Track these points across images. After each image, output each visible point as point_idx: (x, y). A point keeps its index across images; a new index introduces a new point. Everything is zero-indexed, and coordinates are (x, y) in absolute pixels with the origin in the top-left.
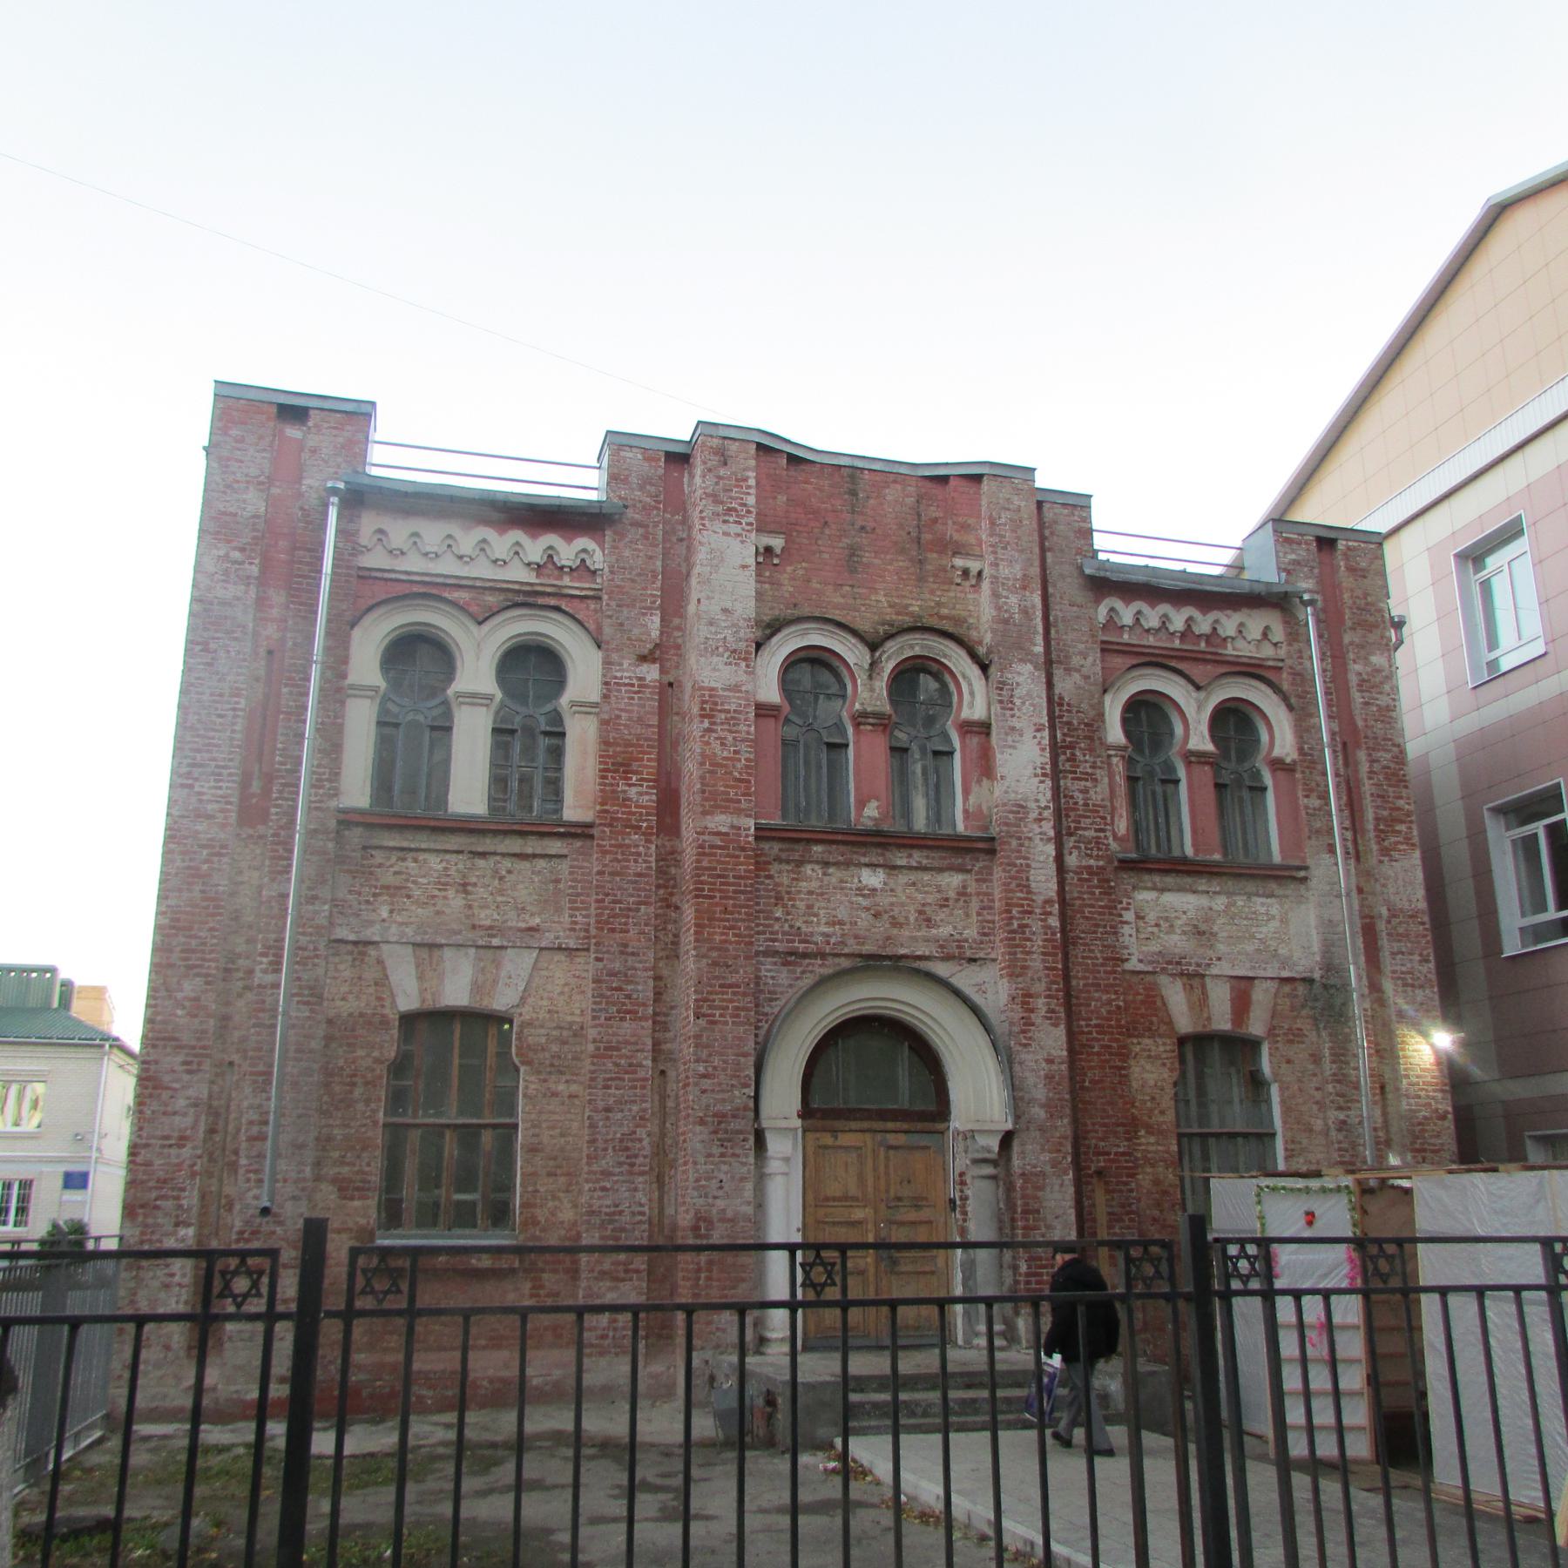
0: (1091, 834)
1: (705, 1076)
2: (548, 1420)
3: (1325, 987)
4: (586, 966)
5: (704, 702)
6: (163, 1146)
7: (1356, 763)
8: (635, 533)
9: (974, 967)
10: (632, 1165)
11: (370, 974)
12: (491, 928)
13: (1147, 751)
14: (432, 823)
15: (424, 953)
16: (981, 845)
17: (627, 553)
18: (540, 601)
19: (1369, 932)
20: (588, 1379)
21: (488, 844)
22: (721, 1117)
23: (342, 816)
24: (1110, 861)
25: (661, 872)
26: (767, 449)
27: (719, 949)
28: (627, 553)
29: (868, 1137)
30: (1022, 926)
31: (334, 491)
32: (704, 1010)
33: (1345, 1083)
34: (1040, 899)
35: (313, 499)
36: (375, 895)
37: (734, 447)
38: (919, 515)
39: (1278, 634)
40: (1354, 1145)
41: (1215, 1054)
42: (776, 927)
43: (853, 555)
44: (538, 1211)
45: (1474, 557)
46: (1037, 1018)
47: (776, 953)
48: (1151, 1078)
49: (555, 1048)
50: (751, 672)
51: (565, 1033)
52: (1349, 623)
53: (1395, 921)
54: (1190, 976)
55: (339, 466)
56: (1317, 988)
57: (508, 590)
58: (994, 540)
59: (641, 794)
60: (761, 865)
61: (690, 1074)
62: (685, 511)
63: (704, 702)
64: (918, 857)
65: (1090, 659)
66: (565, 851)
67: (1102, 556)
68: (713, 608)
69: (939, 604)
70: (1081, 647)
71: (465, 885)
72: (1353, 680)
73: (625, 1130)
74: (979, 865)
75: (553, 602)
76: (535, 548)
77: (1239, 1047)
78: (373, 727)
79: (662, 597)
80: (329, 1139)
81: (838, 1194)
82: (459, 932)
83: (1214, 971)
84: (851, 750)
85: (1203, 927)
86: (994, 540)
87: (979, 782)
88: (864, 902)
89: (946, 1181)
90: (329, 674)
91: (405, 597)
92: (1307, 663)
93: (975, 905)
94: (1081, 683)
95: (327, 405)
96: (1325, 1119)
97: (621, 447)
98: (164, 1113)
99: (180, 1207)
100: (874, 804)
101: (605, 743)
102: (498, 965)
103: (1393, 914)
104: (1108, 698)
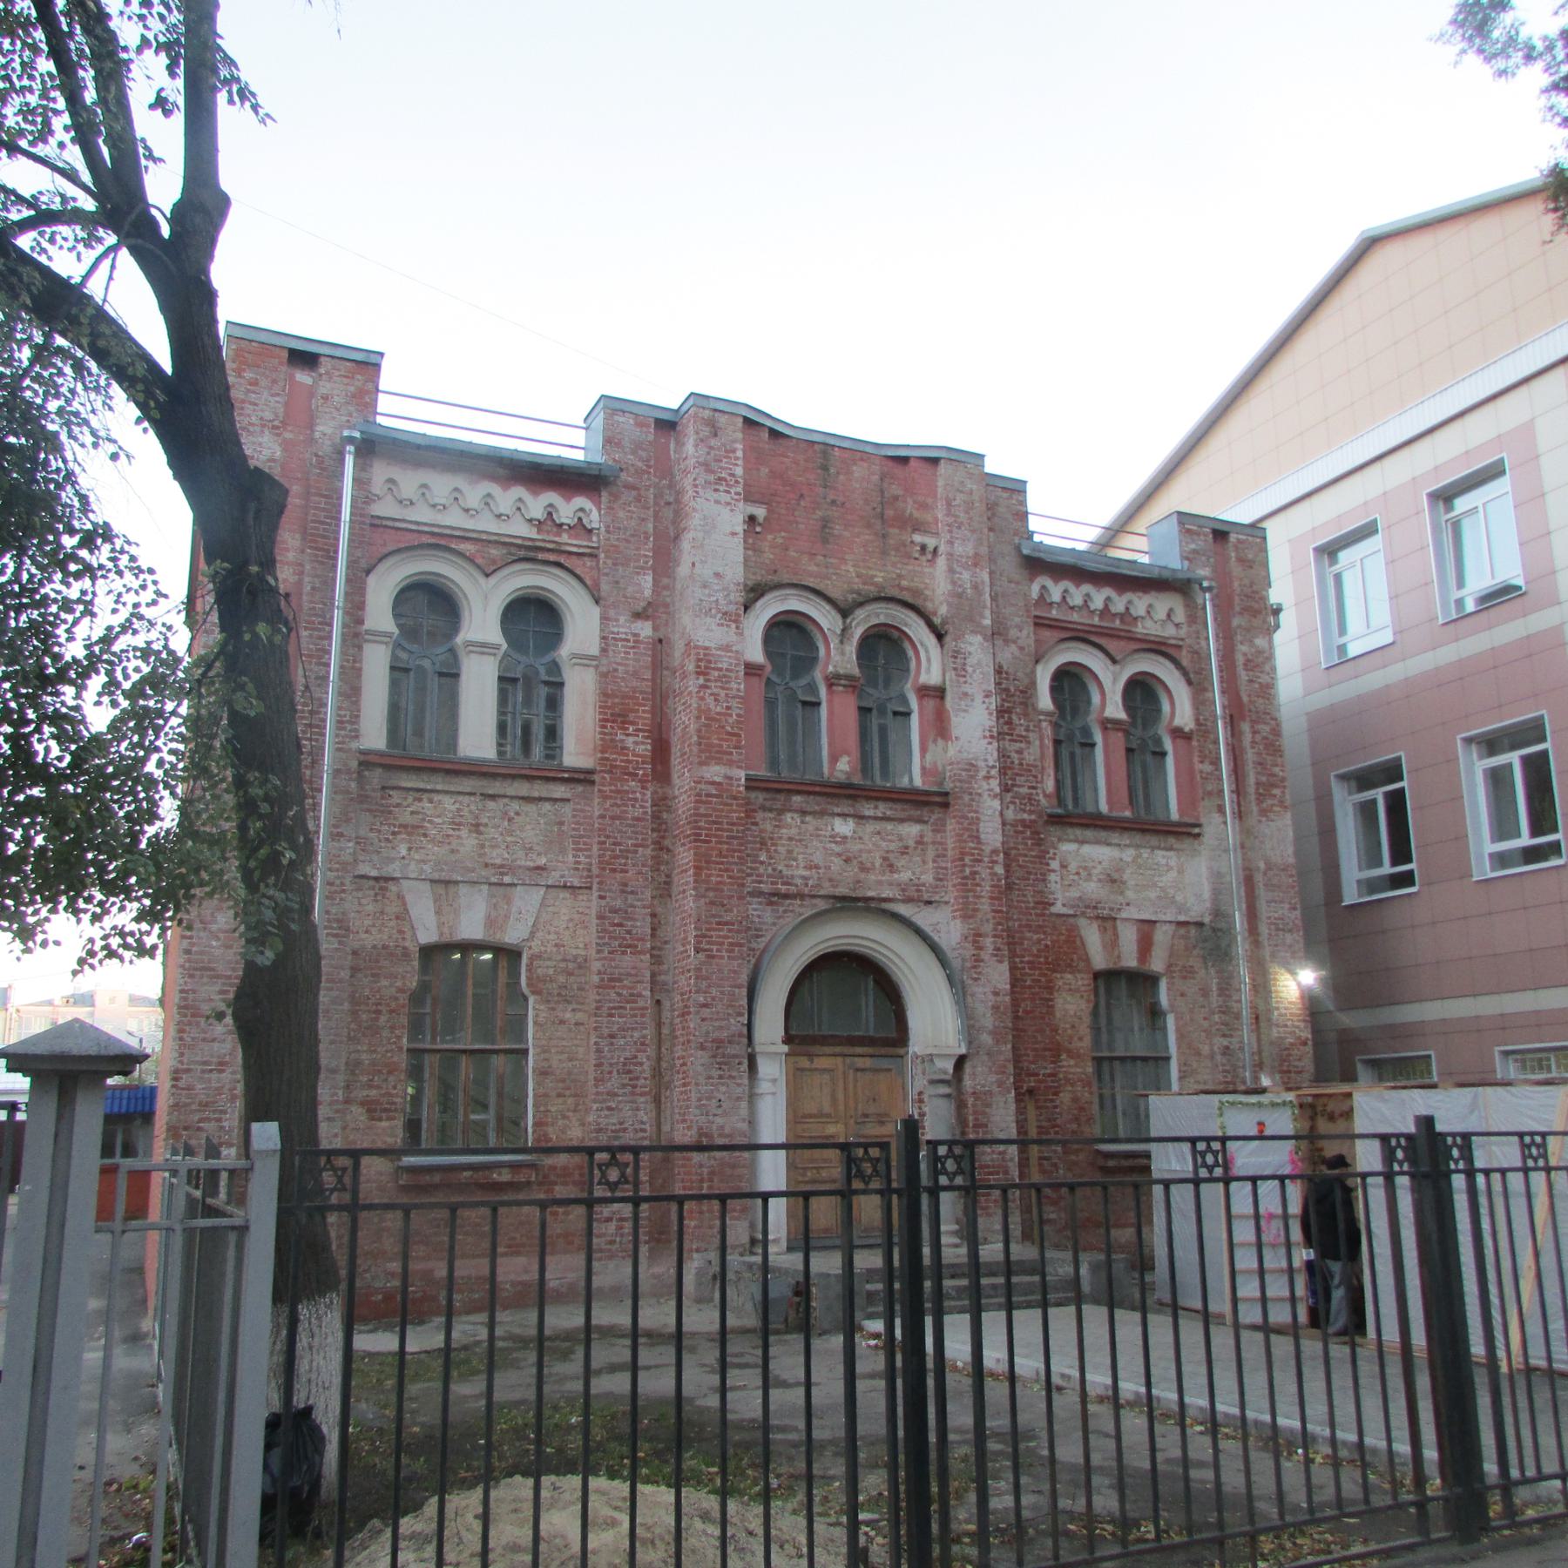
0: (1024, 790)
1: (705, 1005)
2: (516, 1322)
3: (1214, 930)
4: (591, 904)
5: (699, 660)
6: (203, 1071)
7: (1241, 733)
8: (628, 496)
9: (930, 909)
10: (634, 1087)
11: (392, 909)
12: (502, 866)
13: (788, 673)
14: (448, 766)
15: (441, 890)
16: (937, 799)
17: (621, 514)
18: (540, 556)
19: (1249, 881)
20: (597, 1282)
21: (496, 787)
22: (719, 1042)
23: (362, 758)
24: (1040, 816)
25: (656, 817)
26: (753, 423)
27: (716, 890)
28: (621, 514)
29: (840, 1059)
30: (974, 873)
31: (351, 440)
32: (704, 946)
33: (1229, 1015)
34: (988, 849)
35: (326, 448)
36: (394, 833)
37: (723, 419)
38: (882, 492)
39: (1180, 616)
40: (1235, 1067)
41: (1122, 988)
42: (761, 870)
43: (824, 527)
44: (550, 1130)
45: (1329, 551)
46: (985, 955)
47: (760, 894)
48: (1071, 1009)
49: (562, 979)
50: (740, 632)
51: (571, 965)
52: (1237, 609)
53: (1270, 873)
54: (1104, 919)
55: (350, 415)
56: (1207, 932)
57: (505, 544)
58: (950, 520)
59: (636, 743)
60: (750, 813)
61: (691, 1003)
62: (672, 475)
63: (699, 660)
64: (883, 809)
65: (1025, 632)
66: (568, 795)
67: (1037, 538)
68: (705, 572)
69: (900, 576)
70: (1017, 620)
71: (478, 825)
72: (1240, 660)
73: (628, 1054)
74: (935, 817)
75: (552, 557)
76: (537, 504)
77: (1140, 982)
78: (388, 670)
79: (654, 557)
80: (358, 1063)
81: (815, 1111)
82: (473, 870)
83: (1124, 915)
84: (824, 710)
85: (1116, 876)
86: (950, 520)
87: (935, 741)
88: (837, 849)
89: (905, 1099)
90: (347, 619)
91: (421, 546)
92: (1203, 643)
93: (931, 853)
94: (1017, 653)
95: (338, 353)
96: (1212, 1045)
97: (615, 411)
98: (204, 1040)
99: (222, 1128)
100: (845, 759)
101: (605, 695)
102: (509, 901)
103: (1269, 866)
104: (1039, 668)
